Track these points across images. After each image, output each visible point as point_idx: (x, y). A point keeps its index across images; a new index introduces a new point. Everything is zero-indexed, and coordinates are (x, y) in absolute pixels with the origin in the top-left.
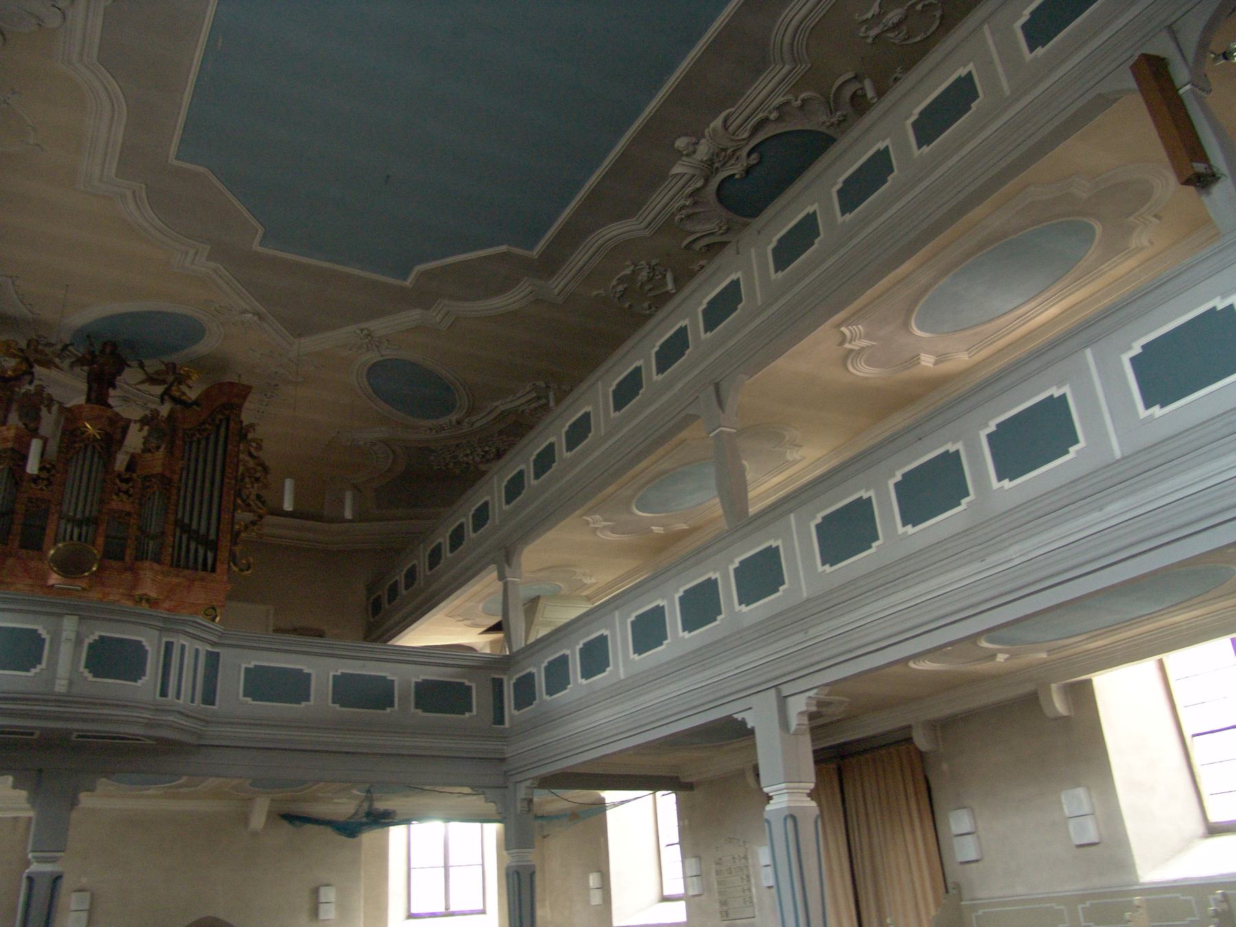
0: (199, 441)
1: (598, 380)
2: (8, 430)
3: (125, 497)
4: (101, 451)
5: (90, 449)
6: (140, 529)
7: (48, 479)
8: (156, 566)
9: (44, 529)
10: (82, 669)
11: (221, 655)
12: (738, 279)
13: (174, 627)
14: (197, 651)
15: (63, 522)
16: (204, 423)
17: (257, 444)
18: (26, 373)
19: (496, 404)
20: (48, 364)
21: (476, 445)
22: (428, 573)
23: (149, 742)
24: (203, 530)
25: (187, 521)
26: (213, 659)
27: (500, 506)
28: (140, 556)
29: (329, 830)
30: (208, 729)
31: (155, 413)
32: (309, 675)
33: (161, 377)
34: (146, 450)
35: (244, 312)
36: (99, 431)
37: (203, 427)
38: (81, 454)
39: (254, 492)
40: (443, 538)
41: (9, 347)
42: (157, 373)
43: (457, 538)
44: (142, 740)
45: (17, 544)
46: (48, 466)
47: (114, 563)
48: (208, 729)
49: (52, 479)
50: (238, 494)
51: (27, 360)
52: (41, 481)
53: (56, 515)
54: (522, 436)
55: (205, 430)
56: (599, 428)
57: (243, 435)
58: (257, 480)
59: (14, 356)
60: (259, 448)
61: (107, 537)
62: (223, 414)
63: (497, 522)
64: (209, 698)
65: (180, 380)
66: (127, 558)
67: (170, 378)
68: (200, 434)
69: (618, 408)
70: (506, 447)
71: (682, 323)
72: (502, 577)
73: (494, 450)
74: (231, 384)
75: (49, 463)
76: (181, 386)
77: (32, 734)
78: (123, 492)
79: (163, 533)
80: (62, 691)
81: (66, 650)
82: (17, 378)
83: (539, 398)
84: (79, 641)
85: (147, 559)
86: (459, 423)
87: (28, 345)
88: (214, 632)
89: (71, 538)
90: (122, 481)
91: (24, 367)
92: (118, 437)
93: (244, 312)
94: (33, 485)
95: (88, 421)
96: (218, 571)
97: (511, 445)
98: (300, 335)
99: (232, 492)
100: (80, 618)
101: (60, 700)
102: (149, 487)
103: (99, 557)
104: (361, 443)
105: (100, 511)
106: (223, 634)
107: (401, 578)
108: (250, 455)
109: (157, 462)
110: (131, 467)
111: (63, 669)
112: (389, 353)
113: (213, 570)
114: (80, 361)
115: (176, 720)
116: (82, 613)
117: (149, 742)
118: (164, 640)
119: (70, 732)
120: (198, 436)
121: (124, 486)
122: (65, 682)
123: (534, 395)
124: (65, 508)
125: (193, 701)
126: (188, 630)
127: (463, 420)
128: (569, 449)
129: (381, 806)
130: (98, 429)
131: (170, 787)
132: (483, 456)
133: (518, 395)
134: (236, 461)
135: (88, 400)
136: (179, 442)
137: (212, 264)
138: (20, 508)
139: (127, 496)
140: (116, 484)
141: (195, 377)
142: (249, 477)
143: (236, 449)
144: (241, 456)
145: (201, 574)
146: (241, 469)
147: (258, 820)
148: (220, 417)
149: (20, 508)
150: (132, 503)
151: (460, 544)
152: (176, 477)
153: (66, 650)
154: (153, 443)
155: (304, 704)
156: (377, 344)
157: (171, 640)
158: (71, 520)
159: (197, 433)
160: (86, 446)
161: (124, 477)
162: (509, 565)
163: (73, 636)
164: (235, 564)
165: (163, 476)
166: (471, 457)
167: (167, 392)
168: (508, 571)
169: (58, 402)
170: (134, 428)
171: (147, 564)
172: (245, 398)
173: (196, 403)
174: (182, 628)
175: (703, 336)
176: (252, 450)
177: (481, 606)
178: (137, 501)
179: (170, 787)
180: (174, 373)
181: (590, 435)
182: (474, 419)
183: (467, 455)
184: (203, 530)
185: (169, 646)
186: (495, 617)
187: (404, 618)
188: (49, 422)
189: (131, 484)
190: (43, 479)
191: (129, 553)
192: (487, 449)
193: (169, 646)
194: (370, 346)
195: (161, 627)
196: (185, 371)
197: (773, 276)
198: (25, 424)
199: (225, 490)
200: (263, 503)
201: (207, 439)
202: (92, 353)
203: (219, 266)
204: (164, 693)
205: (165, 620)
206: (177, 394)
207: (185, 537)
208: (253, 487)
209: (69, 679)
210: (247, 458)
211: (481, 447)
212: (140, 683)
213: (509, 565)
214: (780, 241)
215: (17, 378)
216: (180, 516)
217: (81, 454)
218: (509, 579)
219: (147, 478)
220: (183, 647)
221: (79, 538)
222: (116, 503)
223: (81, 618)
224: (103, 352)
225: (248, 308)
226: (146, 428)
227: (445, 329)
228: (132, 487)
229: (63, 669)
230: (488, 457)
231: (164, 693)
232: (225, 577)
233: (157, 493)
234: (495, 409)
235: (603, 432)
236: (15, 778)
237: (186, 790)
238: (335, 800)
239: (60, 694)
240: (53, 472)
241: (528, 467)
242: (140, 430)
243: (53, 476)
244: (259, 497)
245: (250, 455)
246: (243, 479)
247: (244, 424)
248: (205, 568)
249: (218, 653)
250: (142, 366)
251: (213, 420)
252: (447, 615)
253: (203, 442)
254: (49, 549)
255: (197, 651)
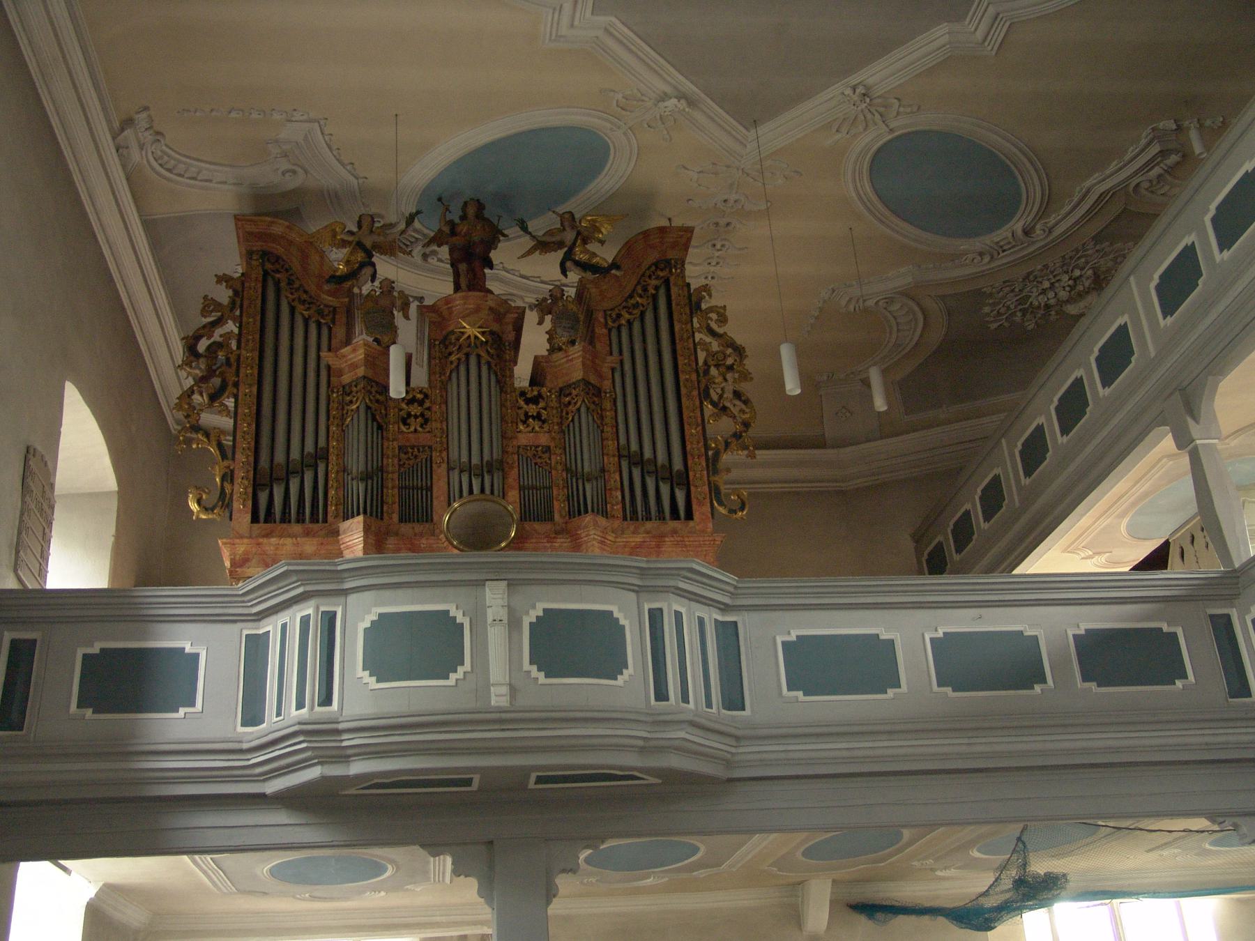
0: (630, 323)
1: (1129, 275)
2: (354, 350)
3: (536, 424)
4: (490, 360)
5: (473, 360)
6: (568, 470)
7: (422, 415)
8: (602, 521)
9: (430, 489)
10: (526, 665)
11: (740, 626)
12: (1126, 324)
13: (659, 582)
14: (701, 622)
15: (455, 475)
16: (631, 296)
17: (718, 313)
18: (362, 265)
19: (1088, 184)
20: (390, 249)
21: (1059, 270)
22: (1025, 481)
23: (652, 780)
24: (661, 457)
25: (634, 447)
26: (729, 633)
27: (1018, 481)
28: (577, 509)
29: (942, 920)
30: (741, 750)
31: (557, 295)
32: (892, 642)
33: (557, 238)
34: (552, 350)
35: (664, 97)
36: (481, 330)
37: (632, 301)
38: (462, 369)
39: (729, 388)
40: (1045, 415)
41: (334, 234)
42: (550, 233)
43: (1034, 451)
44: (643, 779)
45: (395, 517)
46: (419, 396)
47: (537, 526)
48: (741, 750)
49: (427, 413)
50: (705, 394)
51: (360, 245)
52: (412, 419)
53: (444, 466)
54: (1137, 238)
55: (636, 306)
56: (1145, 345)
57: (694, 306)
58: (730, 368)
59: (344, 244)
60: (723, 319)
61: (522, 488)
62: (658, 278)
63: (1152, 351)
64: (734, 700)
65: (584, 237)
66: (557, 516)
67: (569, 236)
68: (630, 314)
69: (1168, 310)
70: (1110, 264)
71: (1120, 321)
72: (1183, 440)
73: (1090, 272)
74: (662, 230)
75: (421, 392)
76: (588, 247)
77: (468, 782)
78: (533, 418)
79: (603, 470)
80: (502, 704)
81: (496, 638)
82: (353, 275)
83: (1163, 153)
84: (513, 623)
85: (586, 512)
86: (1027, 232)
87: (360, 226)
88: (723, 586)
89: (471, 492)
90: (528, 401)
91: (360, 256)
92: (511, 336)
93: (664, 97)
94: (403, 428)
95: (463, 318)
96: (696, 515)
97: (1119, 259)
98: (755, 123)
99: (695, 393)
100: (509, 585)
101: (501, 720)
102: (569, 403)
103: (516, 517)
104: (871, 303)
105: (504, 452)
106: (736, 587)
107: (973, 504)
108: (712, 333)
109: (573, 364)
110: (535, 380)
111: (498, 670)
112: (902, 124)
113: (689, 516)
114: (438, 240)
115: (688, 737)
116: (510, 576)
117: (652, 780)
118: (646, 607)
119: (525, 771)
120: (627, 316)
121: (532, 410)
122: (504, 690)
123: (1155, 149)
124: (454, 454)
125: (709, 705)
126: (682, 585)
127: (1034, 227)
128: (1106, 382)
129: (1040, 866)
130: (479, 327)
131: (679, 870)
132: (1072, 288)
133: (1127, 158)
134: (691, 346)
135: (457, 288)
136: (600, 331)
137: (603, 20)
138: (391, 463)
139: (540, 423)
140: (520, 408)
141: (606, 229)
142: (717, 366)
143: (689, 326)
144: (698, 336)
145: (673, 524)
146: (702, 356)
147: (818, 915)
148: (654, 282)
149: (391, 463)
150: (549, 432)
151: (969, 539)
152: (607, 384)
153: (496, 638)
154: (563, 338)
155: (891, 692)
156: (882, 109)
157: (656, 605)
158: (469, 469)
159: (624, 313)
160: (467, 355)
161: (529, 396)
162: (1196, 420)
163: (503, 614)
164: (721, 503)
165: (586, 382)
166: (1051, 294)
167: (568, 256)
168: (1194, 429)
169: (416, 298)
170: (531, 317)
171: (588, 519)
172: (686, 247)
173: (615, 265)
174: (672, 583)
175: (1218, 257)
176: (714, 326)
177: (1125, 522)
178: (556, 427)
179: (679, 870)
180: (573, 227)
181: (1048, 455)
182: (1052, 220)
183: (1044, 292)
184: (661, 457)
185: (656, 617)
186: (1147, 543)
187: (1020, 539)
188: (408, 330)
189: (542, 404)
190: (416, 417)
191: (559, 507)
192: (1077, 273)
193: (656, 617)
194: (869, 116)
195: (638, 586)
196: (589, 221)
197: (1162, 323)
198: (376, 340)
199: (683, 391)
200: (746, 402)
201: (642, 314)
202: (452, 224)
203: (613, 19)
204: (661, 695)
205: (643, 572)
206: (583, 257)
207: (636, 473)
208: (725, 380)
209: (510, 685)
210: (708, 339)
211: (1067, 272)
212: (621, 680)
213: (1196, 420)
214: (1060, 400)
215: (353, 275)
216: (623, 441)
217: (462, 369)
218: (1198, 442)
219: (562, 392)
220: (678, 615)
221: (482, 491)
222: (524, 437)
223: (511, 584)
224: (464, 218)
225: (668, 90)
226: (548, 318)
227: (994, 53)
228: (545, 409)
229: (498, 670)
230: (1080, 288)
231: (661, 695)
232: (710, 525)
233: (583, 410)
234: (1088, 191)
235: (1152, 351)
236: (453, 856)
237: (702, 873)
238: (939, 873)
239: (500, 710)
240: (427, 404)
241: (974, 505)
242: (541, 323)
243: (429, 409)
244: (737, 394)
245: (712, 333)
246: (706, 372)
247: (693, 287)
248: (675, 514)
249: (735, 623)
250: (524, 229)
251: (645, 290)
252: (1065, 551)
253: (636, 326)
254: (442, 516)
255: (701, 622)
